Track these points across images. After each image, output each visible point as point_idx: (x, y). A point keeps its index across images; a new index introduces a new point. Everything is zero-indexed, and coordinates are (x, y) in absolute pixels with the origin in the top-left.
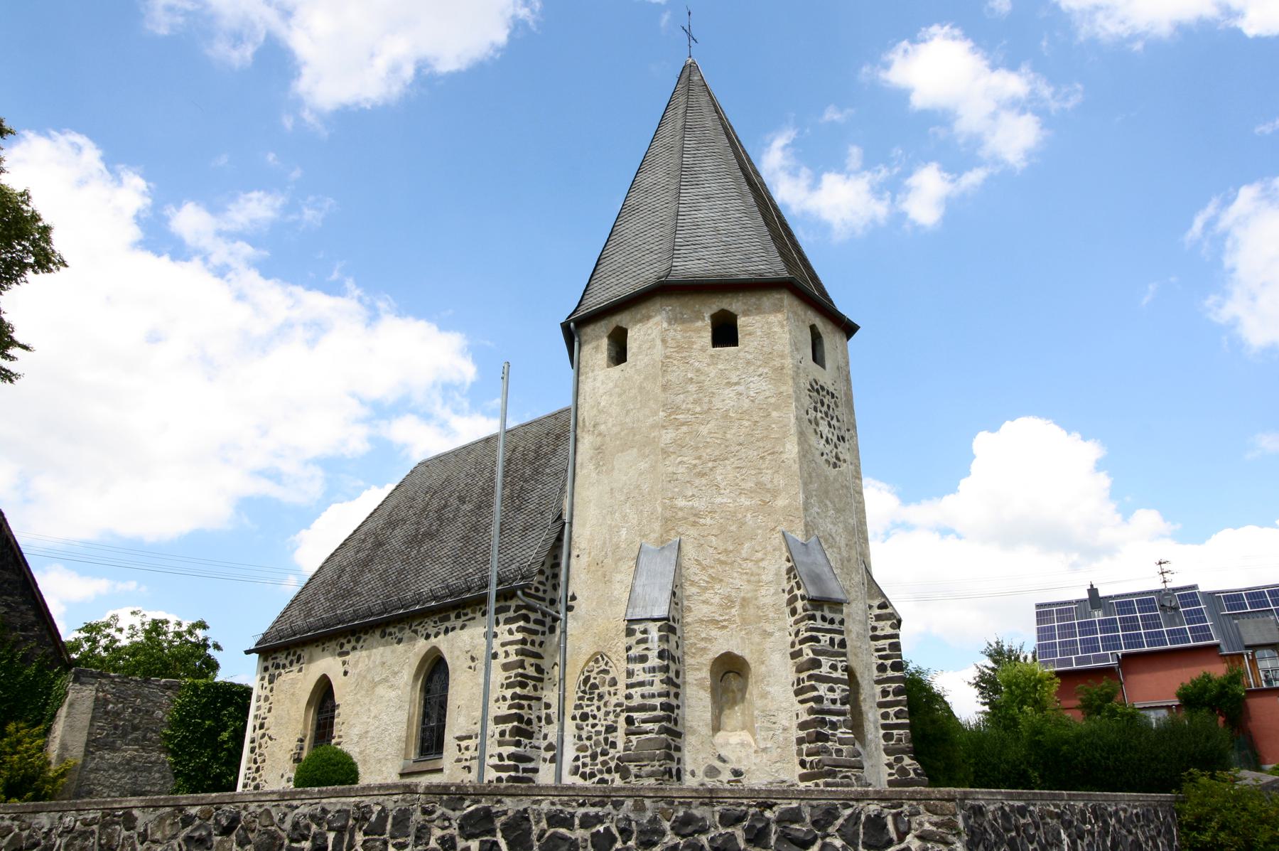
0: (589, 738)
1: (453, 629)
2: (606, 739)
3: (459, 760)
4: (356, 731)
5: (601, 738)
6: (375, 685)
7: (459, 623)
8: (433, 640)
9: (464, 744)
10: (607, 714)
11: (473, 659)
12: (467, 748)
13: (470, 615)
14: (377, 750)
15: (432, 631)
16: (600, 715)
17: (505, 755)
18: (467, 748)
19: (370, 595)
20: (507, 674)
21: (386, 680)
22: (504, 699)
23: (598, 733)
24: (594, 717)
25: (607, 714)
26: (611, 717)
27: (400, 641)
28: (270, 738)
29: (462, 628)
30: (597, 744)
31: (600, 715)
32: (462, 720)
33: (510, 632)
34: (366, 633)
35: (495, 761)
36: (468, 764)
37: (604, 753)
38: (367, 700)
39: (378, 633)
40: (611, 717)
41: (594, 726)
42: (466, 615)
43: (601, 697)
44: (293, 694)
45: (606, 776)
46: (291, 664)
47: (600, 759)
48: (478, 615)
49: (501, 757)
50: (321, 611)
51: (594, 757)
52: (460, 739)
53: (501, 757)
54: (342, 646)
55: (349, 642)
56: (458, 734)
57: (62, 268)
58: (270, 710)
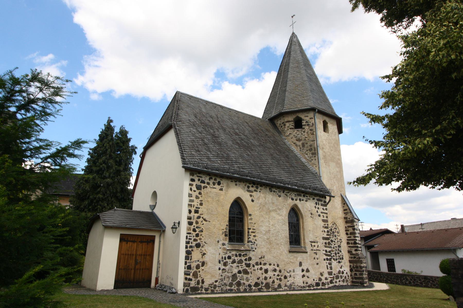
0: (334, 248)
1: (303, 200)
2: (338, 249)
3: (312, 250)
4: (263, 229)
5: (337, 248)
6: (270, 211)
7: (305, 199)
8: (295, 202)
9: (313, 244)
10: (338, 241)
11: (311, 214)
12: (314, 246)
13: (309, 198)
14: (276, 239)
15: (295, 198)
16: (336, 241)
17: (328, 251)
18: (314, 246)
19: (162, 129)
20: (324, 223)
21: (275, 210)
22: (325, 231)
23: (336, 247)
24: (335, 242)
25: (338, 241)
26: (339, 242)
27: (280, 196)
28: (205, 220)
29: (306, 201)
30: (336, 250)
31: (336, 241)
32: (311, 235)
33: (323, 209)
34: (261, 186)
35: (324, 252)
36: (315, 252)
37: (338, 253)
38: (267, 217)
39: (268, 189)
40: (339, 242)
41: (335, 244)
42: (307, 197)
43: (335, 236)
44: (218, 201)
45: (340, 260)
46: (214, 184)
47: (338, 255)
48: (312, 199)
49: (326, 251)
50: (157, 133)
51: (336, 254)
52: (311, 242)
53: (326, 251)
54: (248, 187)
55: (252, 187)
56: (310, 240)
57: (351, 6)
58: (201, 204)
